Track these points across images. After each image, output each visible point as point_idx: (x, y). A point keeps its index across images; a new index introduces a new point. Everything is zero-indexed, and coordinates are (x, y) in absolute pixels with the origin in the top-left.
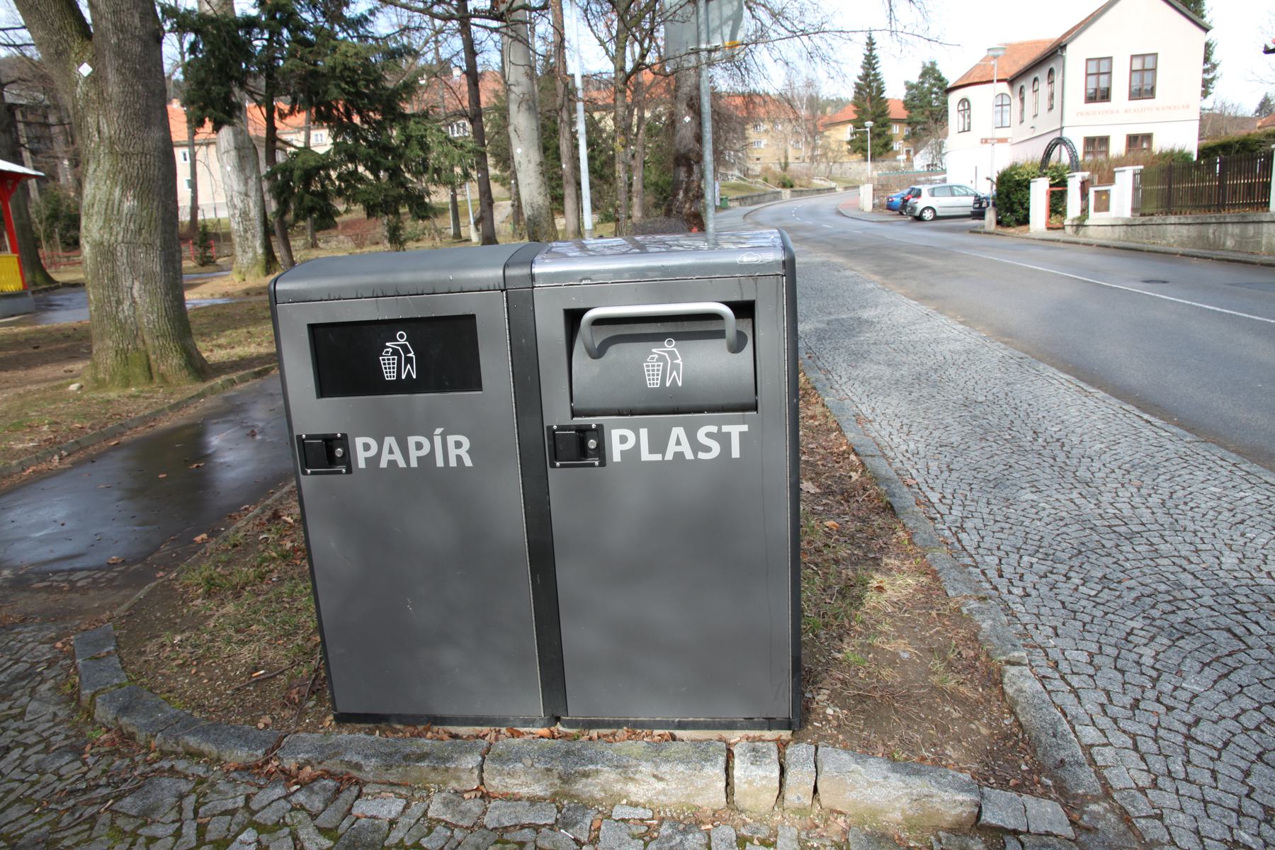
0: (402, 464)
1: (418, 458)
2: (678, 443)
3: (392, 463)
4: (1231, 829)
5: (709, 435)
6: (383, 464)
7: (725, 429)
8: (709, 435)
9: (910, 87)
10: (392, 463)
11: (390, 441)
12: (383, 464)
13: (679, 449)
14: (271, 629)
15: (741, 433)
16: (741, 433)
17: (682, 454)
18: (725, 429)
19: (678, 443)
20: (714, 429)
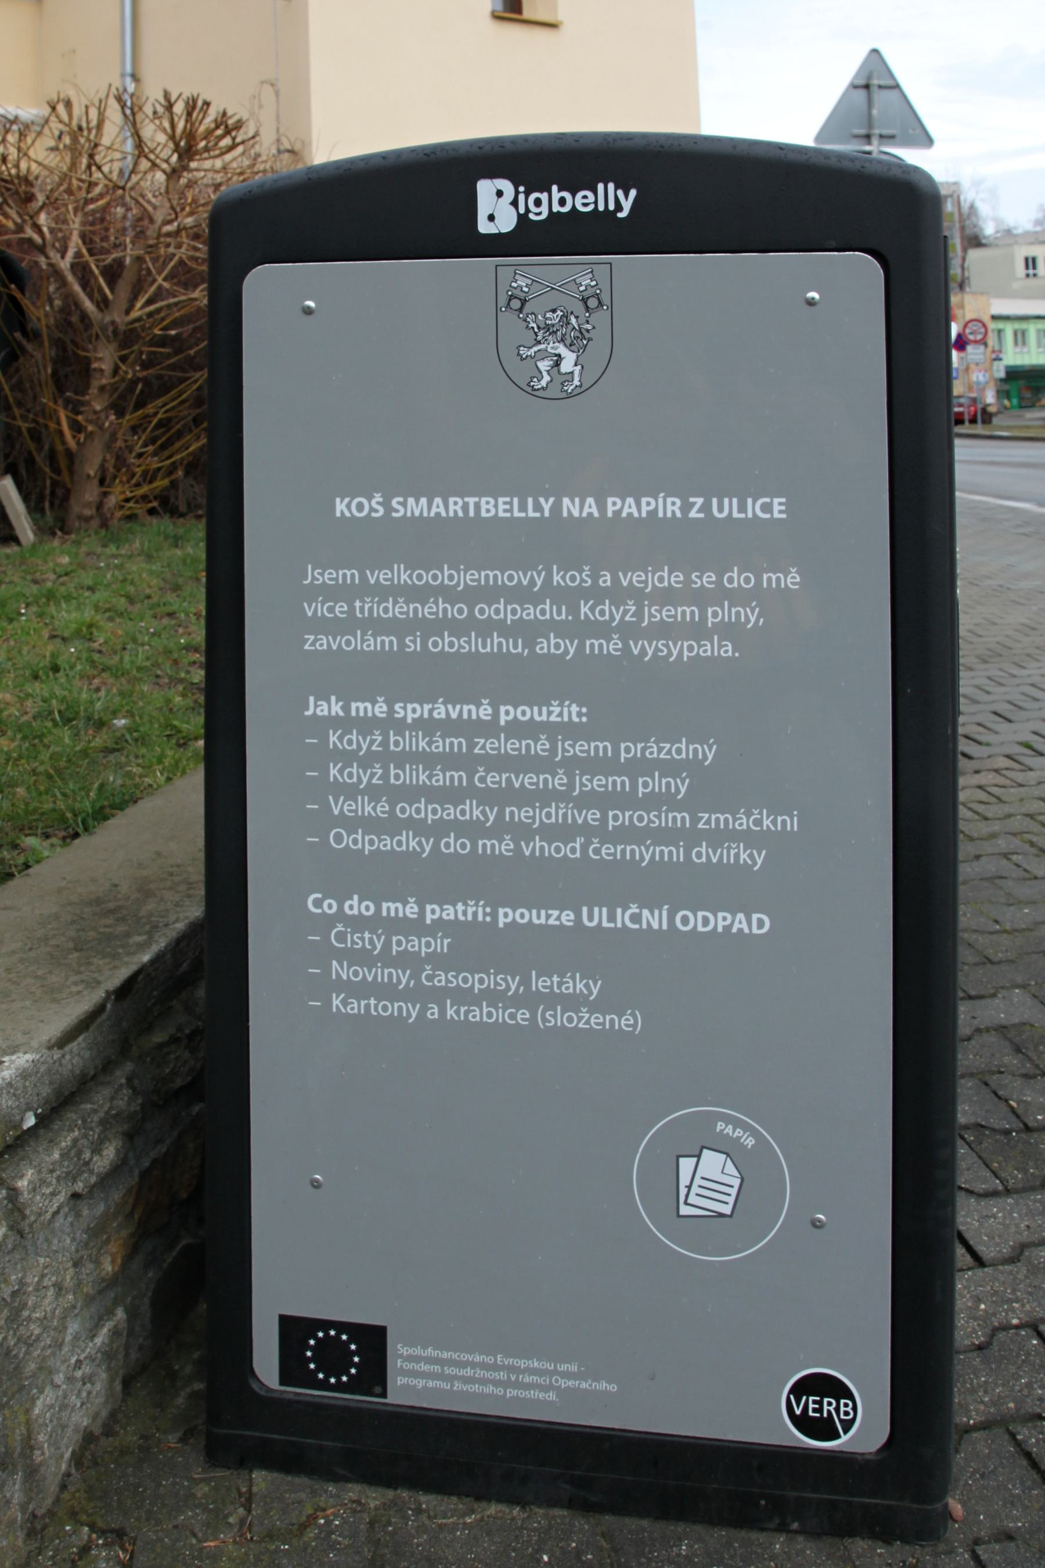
6: (624, 515)
8: (398, 503)
10: (630, 514)
12: (624, 515)
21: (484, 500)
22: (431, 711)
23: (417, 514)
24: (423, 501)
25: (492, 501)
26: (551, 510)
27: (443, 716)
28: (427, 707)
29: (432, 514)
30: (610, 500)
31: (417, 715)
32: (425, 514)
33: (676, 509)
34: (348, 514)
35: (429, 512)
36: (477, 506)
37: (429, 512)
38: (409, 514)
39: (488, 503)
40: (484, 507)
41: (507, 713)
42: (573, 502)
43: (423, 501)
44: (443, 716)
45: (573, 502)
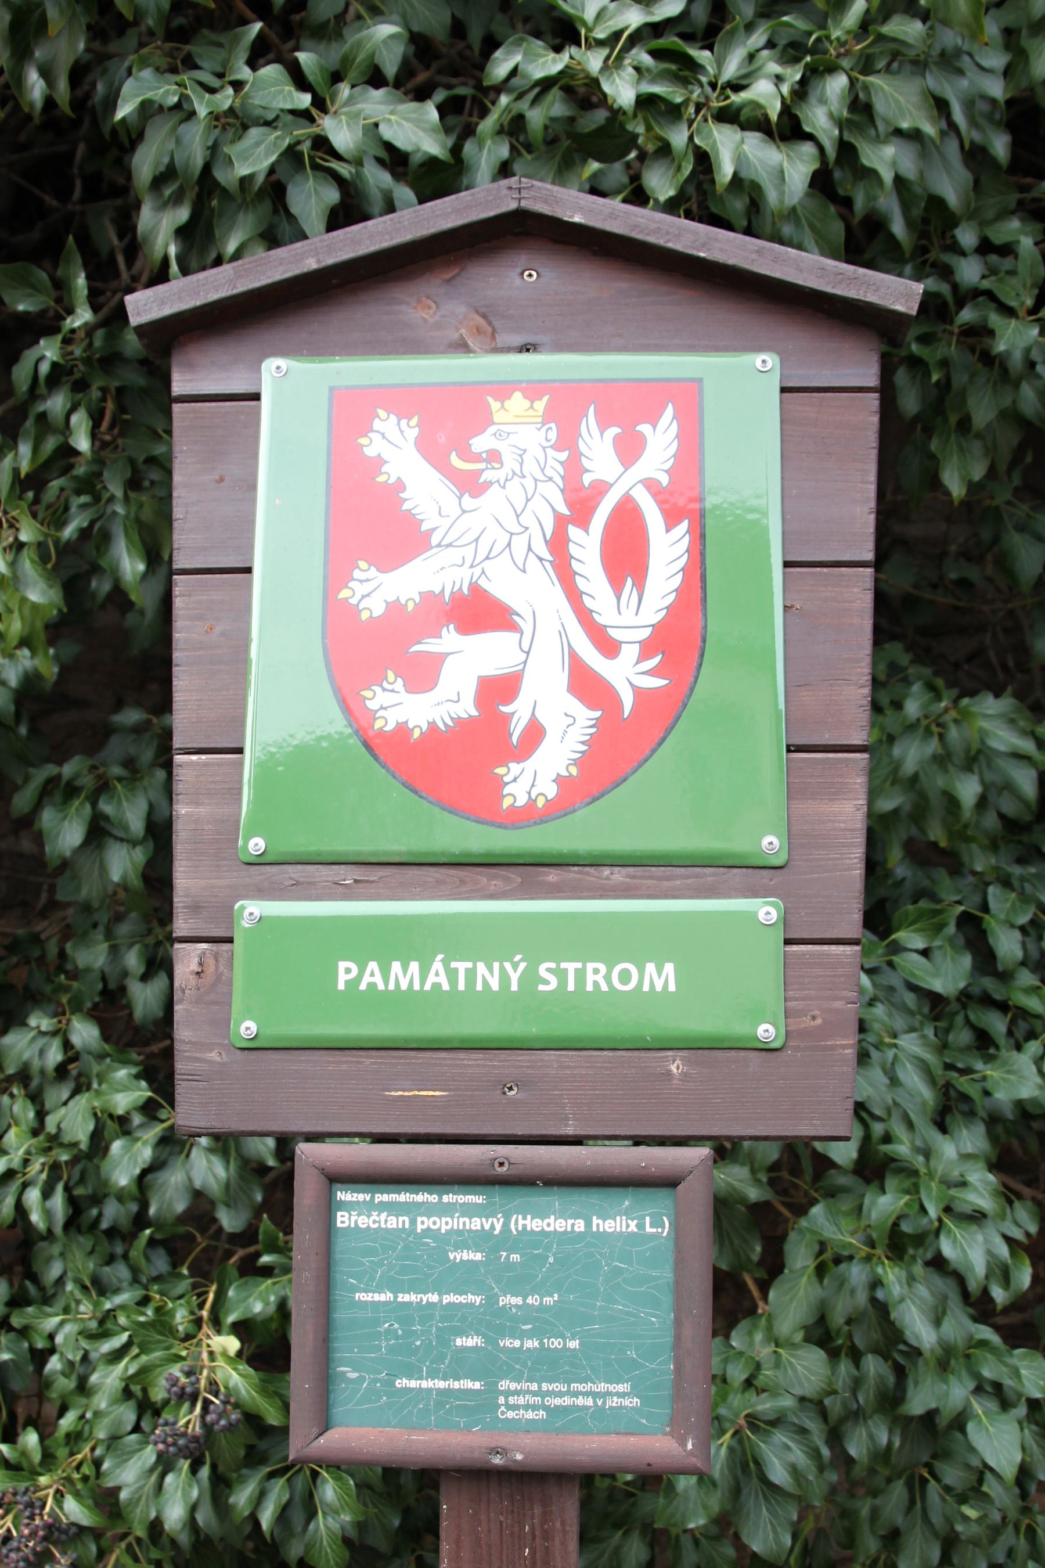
0: (381, 986)
1: (346, 982)
2: (372, 974)
3: (372, 986)
4: (778, 1364)
5: (548, 970)
6: (363, 986)
7: (563, 965)
8: (548, 970)
9: (432, 726)
10: (372, 986)
11: (373, 966)
12: (363, 986)
13: (372, 980)
14: (898, 1243)
15: (467, 970)
16: (467, 970)
17: (374, 984)
18: (563, 965)
19: (437, 974)
20: (553, 965)
21: (590, 966)
22: (573, 1225)
23: (404, 986)
24: (414, 967)
25: (603, 968)
26: (520, 979)
27: (479, 1228)
28: (570, 1222)
29: (428, 987)
30: (342, 965)
31: (449, 1227)
32: (417, 987)
33: (599, 978)
34: (604, 987)
35: (423, 982)
36: (580, 974)
37: (423, 982)
38: (646, 988)
39: (596, 971)
40: (590, 978)
41: (423, 1223)
42: (491, 970)
43: (414, 967)
44: (479, 1228)
45: (491, 970)
